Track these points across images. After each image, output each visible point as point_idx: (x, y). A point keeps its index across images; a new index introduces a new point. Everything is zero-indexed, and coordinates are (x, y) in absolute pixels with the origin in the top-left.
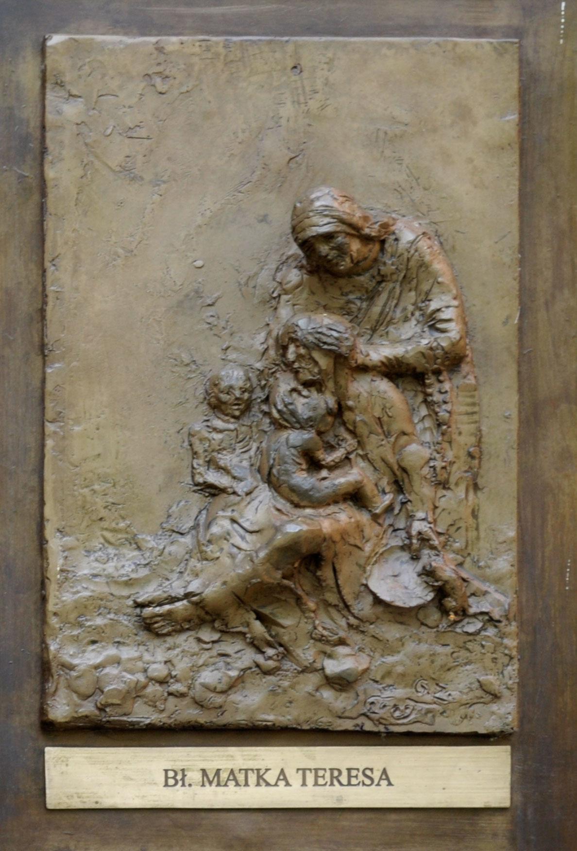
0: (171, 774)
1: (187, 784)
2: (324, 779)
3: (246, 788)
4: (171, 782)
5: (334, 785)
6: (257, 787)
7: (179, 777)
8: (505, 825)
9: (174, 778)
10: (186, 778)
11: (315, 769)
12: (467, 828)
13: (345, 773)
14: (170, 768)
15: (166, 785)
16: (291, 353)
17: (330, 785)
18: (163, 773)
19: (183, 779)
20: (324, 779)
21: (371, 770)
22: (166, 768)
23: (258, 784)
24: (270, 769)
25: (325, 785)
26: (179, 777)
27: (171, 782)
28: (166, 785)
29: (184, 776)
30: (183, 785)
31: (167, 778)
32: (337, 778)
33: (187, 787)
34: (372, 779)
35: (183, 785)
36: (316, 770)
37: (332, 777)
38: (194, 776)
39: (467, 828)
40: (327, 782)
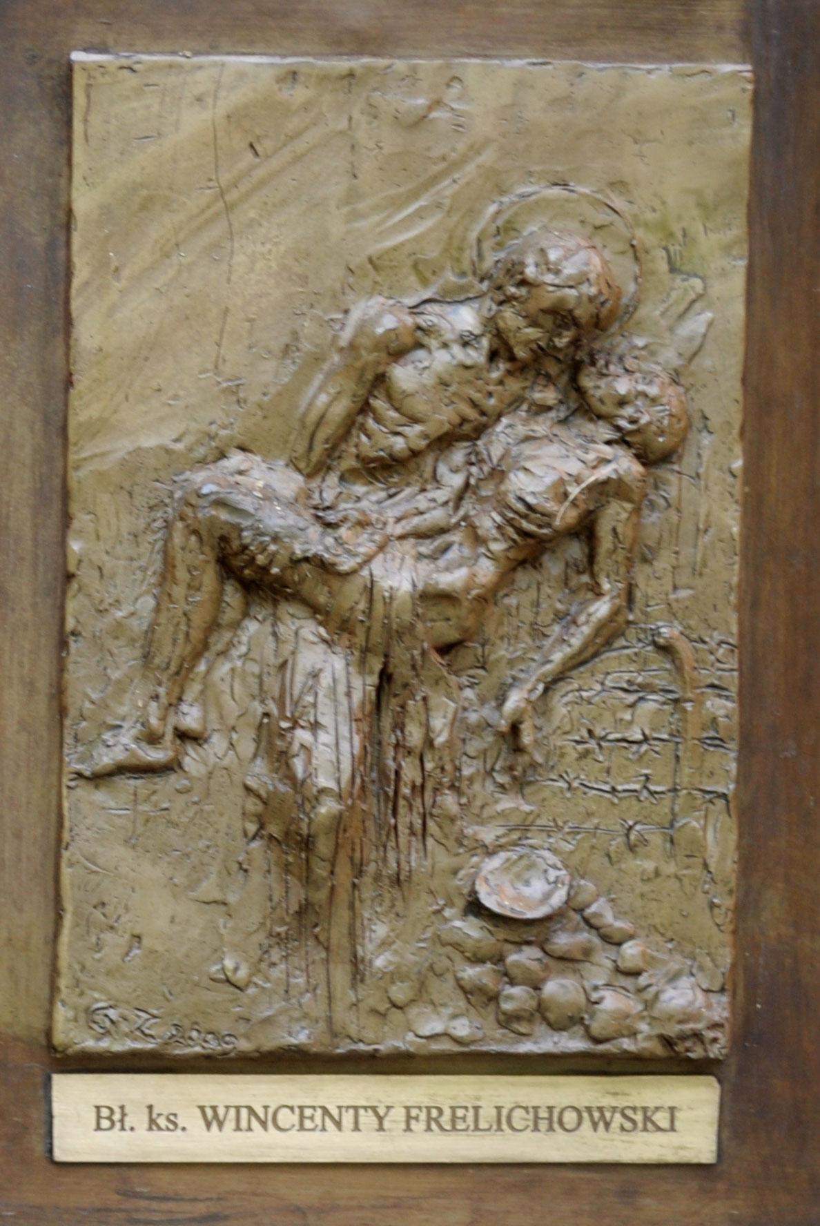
0: (105, 1112)
1: (127, 1126)
2: (465, 1121)
3: (249, 1134)
4: (105, 1124)
5: (554, 1130)
6: (549, 1133)
7: (117, 1117)
8: (734, 13)
9: (109, 1118)
10: (127, 1119)
11: (427, 1107)
12: (680, 17)
13: (447, 1113)
14: (103, 1104)
15: (98, 1128)
16: (123, 1045)
17: (496, 1131)
18: (94, 1110)
19: (122, 1121)
20: (465, 1121)
21: (623, 1129)
22: (98, 1104)
23: (150, 1129)
24: (392, 1107)
25: (466, 1130)
26: (117, 1117)
27: (105, 1124)
28: (98, 1128)
29: (124, 1115)
30: (123, 1129)
31: (99, 1117)
32: (437, 1121)
33: (129, 1132)
34: (634, 1122)
35: (123, 1129)
36: (301, 1108)
37: (429, 1118)
38: (137, 1118)
39: (680, 17)
40: (317, 1126)
